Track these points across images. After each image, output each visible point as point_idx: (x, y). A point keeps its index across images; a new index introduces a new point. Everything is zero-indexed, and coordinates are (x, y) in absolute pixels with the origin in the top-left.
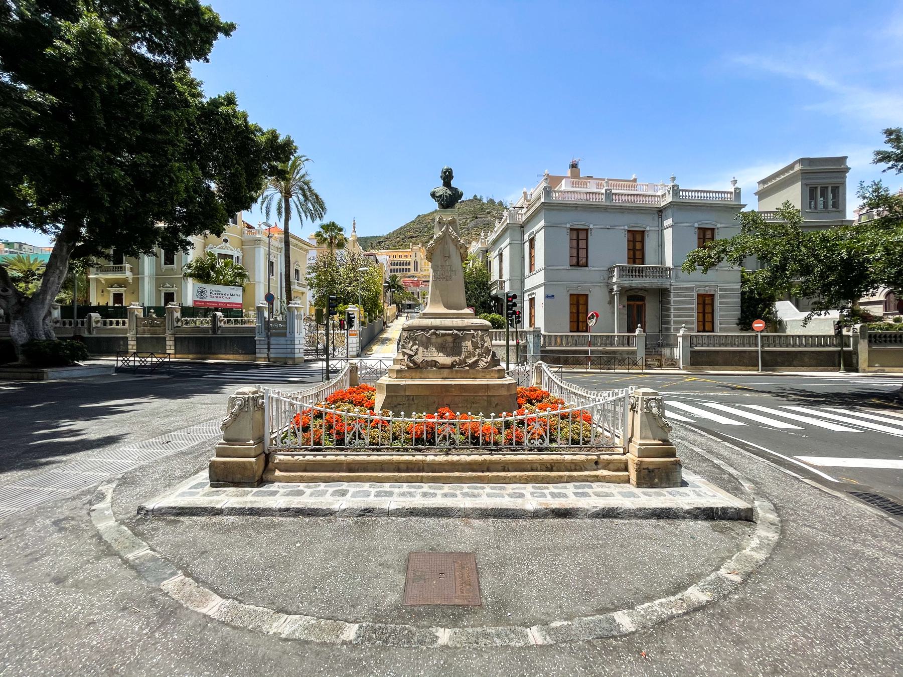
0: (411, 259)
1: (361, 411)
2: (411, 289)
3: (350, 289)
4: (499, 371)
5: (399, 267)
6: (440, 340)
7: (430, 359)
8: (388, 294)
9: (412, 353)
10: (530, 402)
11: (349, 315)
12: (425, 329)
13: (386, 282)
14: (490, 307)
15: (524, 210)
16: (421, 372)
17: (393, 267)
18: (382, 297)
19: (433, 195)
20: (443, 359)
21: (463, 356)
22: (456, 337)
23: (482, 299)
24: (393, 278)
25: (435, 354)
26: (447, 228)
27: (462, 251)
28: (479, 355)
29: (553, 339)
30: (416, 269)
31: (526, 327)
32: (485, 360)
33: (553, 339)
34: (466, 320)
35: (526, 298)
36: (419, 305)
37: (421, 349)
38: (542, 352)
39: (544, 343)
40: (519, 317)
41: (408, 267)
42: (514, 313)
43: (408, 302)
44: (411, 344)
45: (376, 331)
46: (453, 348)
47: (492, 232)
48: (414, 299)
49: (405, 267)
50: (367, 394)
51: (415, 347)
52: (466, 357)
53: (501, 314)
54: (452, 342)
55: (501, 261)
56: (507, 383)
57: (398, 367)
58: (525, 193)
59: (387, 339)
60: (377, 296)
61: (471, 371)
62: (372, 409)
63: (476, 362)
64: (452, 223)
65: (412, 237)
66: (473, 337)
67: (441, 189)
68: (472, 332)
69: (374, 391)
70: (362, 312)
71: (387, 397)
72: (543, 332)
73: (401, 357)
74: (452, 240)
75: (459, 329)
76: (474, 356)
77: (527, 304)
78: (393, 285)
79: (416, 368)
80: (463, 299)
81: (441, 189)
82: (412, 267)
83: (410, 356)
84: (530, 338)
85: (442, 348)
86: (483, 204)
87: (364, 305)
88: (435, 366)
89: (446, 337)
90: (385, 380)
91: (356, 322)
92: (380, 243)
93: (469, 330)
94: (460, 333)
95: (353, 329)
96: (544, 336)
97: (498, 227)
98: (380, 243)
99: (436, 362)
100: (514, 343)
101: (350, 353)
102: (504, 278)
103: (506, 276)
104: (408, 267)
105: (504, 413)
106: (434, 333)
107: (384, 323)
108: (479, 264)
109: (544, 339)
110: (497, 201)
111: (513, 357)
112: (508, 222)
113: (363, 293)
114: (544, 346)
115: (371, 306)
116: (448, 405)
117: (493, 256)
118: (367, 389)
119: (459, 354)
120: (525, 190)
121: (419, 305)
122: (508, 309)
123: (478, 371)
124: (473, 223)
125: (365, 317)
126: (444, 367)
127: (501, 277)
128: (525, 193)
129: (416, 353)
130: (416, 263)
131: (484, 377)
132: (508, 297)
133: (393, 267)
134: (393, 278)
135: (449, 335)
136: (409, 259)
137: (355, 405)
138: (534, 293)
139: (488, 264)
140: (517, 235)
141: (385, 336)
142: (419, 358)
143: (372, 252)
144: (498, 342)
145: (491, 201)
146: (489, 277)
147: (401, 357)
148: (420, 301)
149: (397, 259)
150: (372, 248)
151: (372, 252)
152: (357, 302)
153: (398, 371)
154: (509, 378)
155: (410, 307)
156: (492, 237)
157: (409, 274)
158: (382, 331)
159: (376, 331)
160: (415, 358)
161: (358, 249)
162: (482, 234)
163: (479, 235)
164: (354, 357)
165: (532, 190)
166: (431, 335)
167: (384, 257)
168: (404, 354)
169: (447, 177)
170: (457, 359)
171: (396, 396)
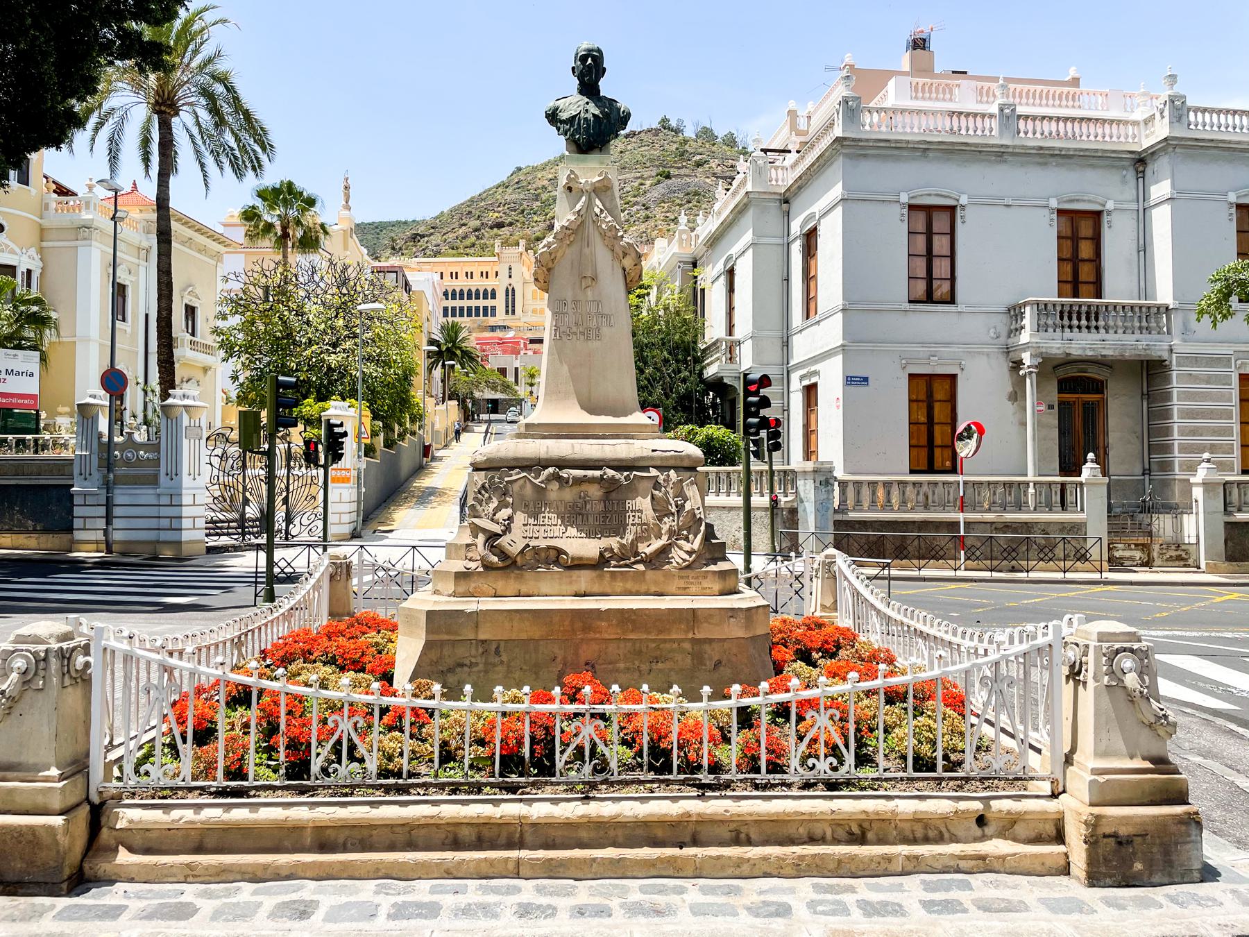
0: (500, 284)
1: (355, 685)
2: (496, 360)
3: (333, 359)
4: (723, 574)
5: (466, 303)
7: (543, 543)
8: (438, 373)
9: (497, 529)
10: (805, 656)
11: (330, 427)
13: (432, 342)
14: (703, 408)
15: (791, 158)
17: (450, 303)
18: (418, 381)
19: (553, 117)
21: (629, 537)
22: (611, 487)
23: (682, 388)
24: (452, 332)
26: (589, 205)
27: (628, 262)
30: (510, 309)
31: (797, 460)
32: (687, 546)
34: (637, 443)
35: (796, 385)
36: (519, 402)
37: (520, 517)
40: (777, 435)
41: (489, 303)
42: (765, 423)
43: (489, 395)
45: (406, 465)
47: (707, 213)
48: (506, 388)
49: (481, 303)
50: (374, 637)
51: (504, 513)
52: (638, 539)
53: (731, 426)
54: (602, 496)
55: (731, 290)
56: (744, 605)
57: (459, 565)
58: (792, 114)
59: (432, 492)
60: (406, 377)
61: (650, 574)
62: (388, 678)
64: (601, 190)
65: (500, 225)
67: (574, 104)
69: (394, 628)
70: (367, 421)
71: (428, 646)
73: (467, 539)
74: (603, 235)
76: (659, 537)
77: (797, 401)
78: (448, 351)
79: (506, 565)
80: (630, 391)
81: (574, 104)
82: (500, 302)
83: (492, 537)
84: (807, 489)
85: (574, 516)
86: (686, 141)
87: (372, 402)
88: (557, 562)
89: (585, 487)
90: (424, 600)
91: (350, 446)
92: (415, 238)
93: (646, 469)
95: (340, 464)
97: (724, 203)
98: (415, 238)
99: (560, 552)
100: (765, 501)
101: (332, 530)
102: (738, 334)
103: (743, 329)
104: (489, 303)
105: (736, 688)
107: (426, 450)
108: (673, 295)
110: (720, 132)
111: (761, 539)
112: (749, 187)
113: (370, 369)
115: (391, 405)
116: (590, 666)
117: (709, 275)
118: (375, 624)
119: (619, 530)
120: (792, 105)
121: (519, 402)
122: (747, 414)
123: (668, 575)
124: (661, 189)
125: (374, 434)
126: (579, 565)
127: (730, 329)
128: (792, 114)
129: (508, 529)
130: (510, 293)
131: (684, 592)
132: (748, 383)
133: (450, 303)
134: (452, 332)
135: (592, 480)
136: (489, 284)
137: (343, 669)
138: (815, 373)
139: (696, 297)
140: (773, 216)
141: (426, 482)
142: (514, 542)
143: (394, 261)
144: (723, 500)
145: (706, 134)
146: (699, 332)
147: (467, 539)
148: (522, 391)
149: (462, 284)
150: (395, 250)
151: (394, 261)
152: (353, 394)
153: (460, 576)
154: (749, 592)
155: (495, 407)
156: (708, 226)
157: (491, 321)
158: (420, 469)
159: (406, 465)
160: (504, 541)
161: (355, 255)
162: (683, 219)
163: (675, 220)
164: (342, 539)
165: (810, 106)
167: (426, 277)
168: (476, 530)
169: (590, 70)
170: (613, 542)
171: (454, 643)
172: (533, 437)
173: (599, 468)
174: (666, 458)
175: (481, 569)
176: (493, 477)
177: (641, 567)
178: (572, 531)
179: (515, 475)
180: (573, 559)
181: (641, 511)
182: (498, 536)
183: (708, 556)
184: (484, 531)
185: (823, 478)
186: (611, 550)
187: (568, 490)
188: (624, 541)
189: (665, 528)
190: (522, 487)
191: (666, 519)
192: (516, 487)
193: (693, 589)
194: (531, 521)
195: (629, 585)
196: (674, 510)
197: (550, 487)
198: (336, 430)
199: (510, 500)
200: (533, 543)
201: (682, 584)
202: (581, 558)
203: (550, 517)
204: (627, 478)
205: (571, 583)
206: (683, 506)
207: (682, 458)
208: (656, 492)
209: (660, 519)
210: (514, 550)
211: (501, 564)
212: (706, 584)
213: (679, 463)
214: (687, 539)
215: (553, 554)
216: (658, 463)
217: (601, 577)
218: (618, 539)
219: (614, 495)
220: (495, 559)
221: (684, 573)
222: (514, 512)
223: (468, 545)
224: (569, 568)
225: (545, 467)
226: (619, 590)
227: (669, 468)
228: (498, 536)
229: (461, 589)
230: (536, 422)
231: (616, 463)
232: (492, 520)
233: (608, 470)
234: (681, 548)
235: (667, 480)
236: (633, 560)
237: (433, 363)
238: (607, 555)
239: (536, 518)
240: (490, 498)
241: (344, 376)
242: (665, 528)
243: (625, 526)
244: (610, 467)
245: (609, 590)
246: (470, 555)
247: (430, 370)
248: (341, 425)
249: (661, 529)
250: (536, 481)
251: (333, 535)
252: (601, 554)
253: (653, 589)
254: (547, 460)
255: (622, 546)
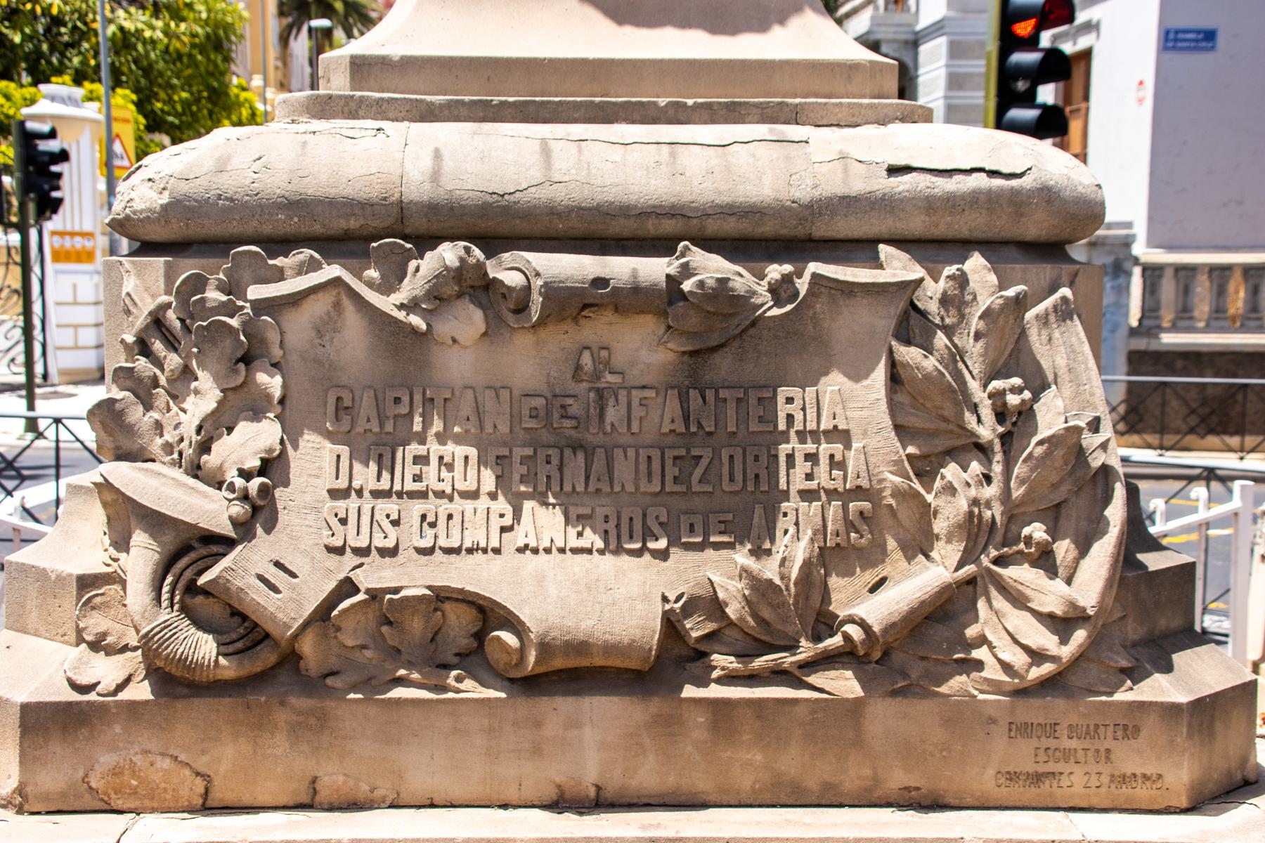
6: (528, 362)
7: (412, 578)
9: (213, 510)
11: (28, 139)
12: (368, 231)
16: (314, 727)
20: (577, 583)
21: (792, 549)
25: (481, 518)
28: (975, 532)
29: (1202, 289)
32: (1051, 594)
33: (1202, 289)
34: (824, 142)
37: (317, 460)
38: (1137, 361)
39: (1150, 309)
44: (205, 396)
46: (685, 452)
51: (250, 440)
52: (831, 557)
61: (885, 716)
63: (945, 614)
66: (912, 324)
68: (897, 266)
72: (1140, 249)
75: (754, 235)
76: (919, 545)
83: (189, 549)
85: (553, 452)
88: (475, 657)
89: (599, 328)
93: (861, 248)
94: (752, 282)
96: (1153, 273)
99: (489, 614)
106: (473, 286)
109: (1151, 289)
114: (1148, 327)
119: (751, 520)
123: (963, 716)
126: (572, 672)
129: (259, 513)
135: (632, 300)
142: (286, 575)
160: (242, 569)
166: (438, 297)
170: (724, 572)
172: (381, 111)
173: (662, 246)
174: (952, 203)
175: (141, 691)
176: (198, 283)
177: (844, 684)
178: (544, 522)
179: (299, 274)
180: (545, 648)
181: (843, 436)
182: (213, 544)
183: (1134, 631)
184: (155, 521)
185: (1109, 260)
186: (712, 605)
187: (524, 341)
188: (769, 570)
189: (949, 513)
190: (326, 328)
191: (951, 472)
192: (299, 325)
193: (1076, 781)
194: (366, 476)
195: (792, 762)
196: (987, 430)
197: (446, 327)
198: (44, 146)
199: (272, 383)
200: (373, 576)
201: (1024, 756)
202: (581, 647)
203: (449, 460)
204: (781, 291)
205: (536, 750)
206: (1026, 414)
207: (1017, 202)
208: (910, 354)
209: (925, 468)
210: (288, 607)
211: (228, 668)
212: (1130, 759)
213: (1002, 226)
214: (1044, 560)
215: (459, 622)
216: (916, 225)
217: (669, 726)
218: (742, 557)
219: (723, 366)
220: (204, 647)
221: (1033, 710)
222: (291, 434)
223: (86, 583)
224: (531, 685)
225: (425, 242)
226: (745, 782)
227: (960, 246)
228: (213, 544)
229: (51, 780)
230: (396, 50)
231: (731, 227)
232: (195, 470)
233: (698, 257)
234: (1019, 600)
235: (956, 300)
236: (807, 649)
237: (290, 28)
238: (696, 628)
239: (386, 463)
240: (187, 373)
241: (84, 36)
242: (949, 513)
243: (772, 499)
244: (709, 244)
245: (702, 783)
246: (96, 623)
247: (284, 40)
248: (52, 135)
249: (927, 513)
250: (387, 304)
251: (62, 373)
252: (671, 625)
253: (897, 779)
254: (432, 208)
255: (761, 590)
